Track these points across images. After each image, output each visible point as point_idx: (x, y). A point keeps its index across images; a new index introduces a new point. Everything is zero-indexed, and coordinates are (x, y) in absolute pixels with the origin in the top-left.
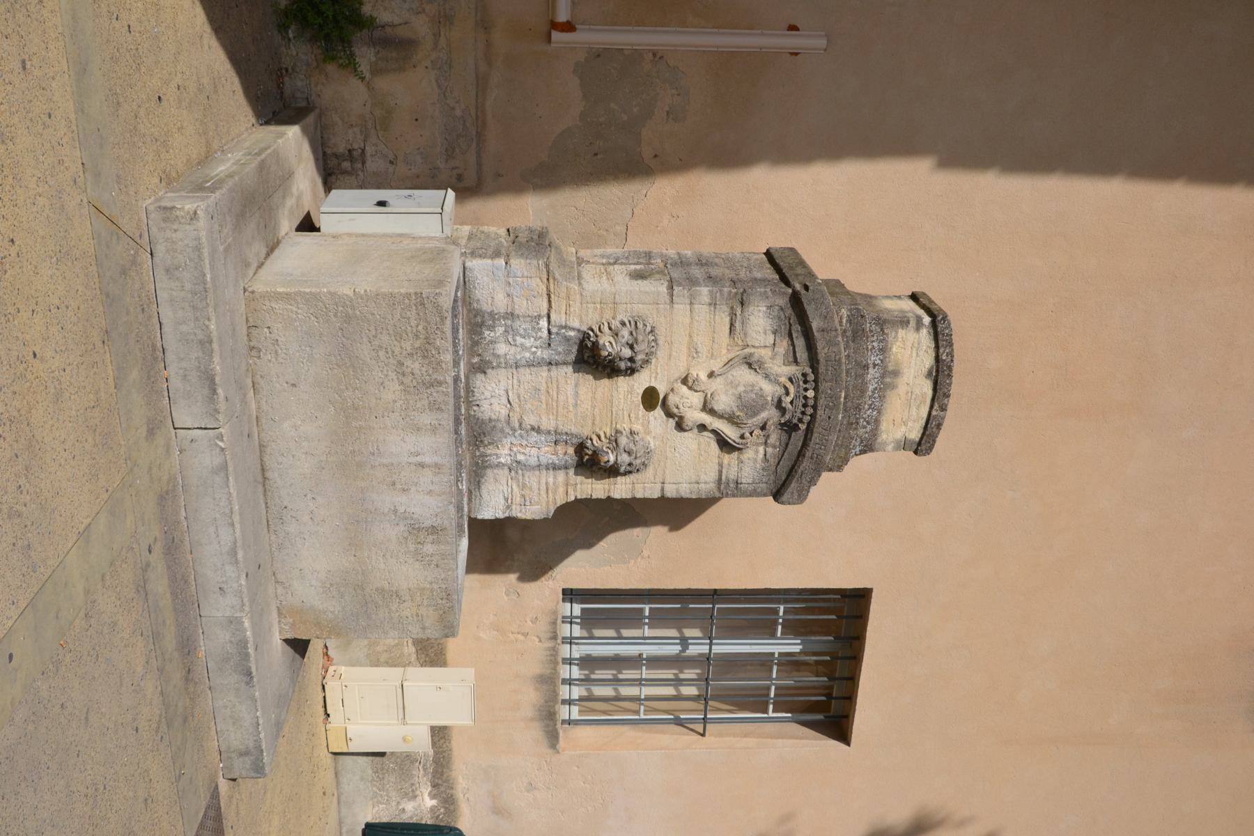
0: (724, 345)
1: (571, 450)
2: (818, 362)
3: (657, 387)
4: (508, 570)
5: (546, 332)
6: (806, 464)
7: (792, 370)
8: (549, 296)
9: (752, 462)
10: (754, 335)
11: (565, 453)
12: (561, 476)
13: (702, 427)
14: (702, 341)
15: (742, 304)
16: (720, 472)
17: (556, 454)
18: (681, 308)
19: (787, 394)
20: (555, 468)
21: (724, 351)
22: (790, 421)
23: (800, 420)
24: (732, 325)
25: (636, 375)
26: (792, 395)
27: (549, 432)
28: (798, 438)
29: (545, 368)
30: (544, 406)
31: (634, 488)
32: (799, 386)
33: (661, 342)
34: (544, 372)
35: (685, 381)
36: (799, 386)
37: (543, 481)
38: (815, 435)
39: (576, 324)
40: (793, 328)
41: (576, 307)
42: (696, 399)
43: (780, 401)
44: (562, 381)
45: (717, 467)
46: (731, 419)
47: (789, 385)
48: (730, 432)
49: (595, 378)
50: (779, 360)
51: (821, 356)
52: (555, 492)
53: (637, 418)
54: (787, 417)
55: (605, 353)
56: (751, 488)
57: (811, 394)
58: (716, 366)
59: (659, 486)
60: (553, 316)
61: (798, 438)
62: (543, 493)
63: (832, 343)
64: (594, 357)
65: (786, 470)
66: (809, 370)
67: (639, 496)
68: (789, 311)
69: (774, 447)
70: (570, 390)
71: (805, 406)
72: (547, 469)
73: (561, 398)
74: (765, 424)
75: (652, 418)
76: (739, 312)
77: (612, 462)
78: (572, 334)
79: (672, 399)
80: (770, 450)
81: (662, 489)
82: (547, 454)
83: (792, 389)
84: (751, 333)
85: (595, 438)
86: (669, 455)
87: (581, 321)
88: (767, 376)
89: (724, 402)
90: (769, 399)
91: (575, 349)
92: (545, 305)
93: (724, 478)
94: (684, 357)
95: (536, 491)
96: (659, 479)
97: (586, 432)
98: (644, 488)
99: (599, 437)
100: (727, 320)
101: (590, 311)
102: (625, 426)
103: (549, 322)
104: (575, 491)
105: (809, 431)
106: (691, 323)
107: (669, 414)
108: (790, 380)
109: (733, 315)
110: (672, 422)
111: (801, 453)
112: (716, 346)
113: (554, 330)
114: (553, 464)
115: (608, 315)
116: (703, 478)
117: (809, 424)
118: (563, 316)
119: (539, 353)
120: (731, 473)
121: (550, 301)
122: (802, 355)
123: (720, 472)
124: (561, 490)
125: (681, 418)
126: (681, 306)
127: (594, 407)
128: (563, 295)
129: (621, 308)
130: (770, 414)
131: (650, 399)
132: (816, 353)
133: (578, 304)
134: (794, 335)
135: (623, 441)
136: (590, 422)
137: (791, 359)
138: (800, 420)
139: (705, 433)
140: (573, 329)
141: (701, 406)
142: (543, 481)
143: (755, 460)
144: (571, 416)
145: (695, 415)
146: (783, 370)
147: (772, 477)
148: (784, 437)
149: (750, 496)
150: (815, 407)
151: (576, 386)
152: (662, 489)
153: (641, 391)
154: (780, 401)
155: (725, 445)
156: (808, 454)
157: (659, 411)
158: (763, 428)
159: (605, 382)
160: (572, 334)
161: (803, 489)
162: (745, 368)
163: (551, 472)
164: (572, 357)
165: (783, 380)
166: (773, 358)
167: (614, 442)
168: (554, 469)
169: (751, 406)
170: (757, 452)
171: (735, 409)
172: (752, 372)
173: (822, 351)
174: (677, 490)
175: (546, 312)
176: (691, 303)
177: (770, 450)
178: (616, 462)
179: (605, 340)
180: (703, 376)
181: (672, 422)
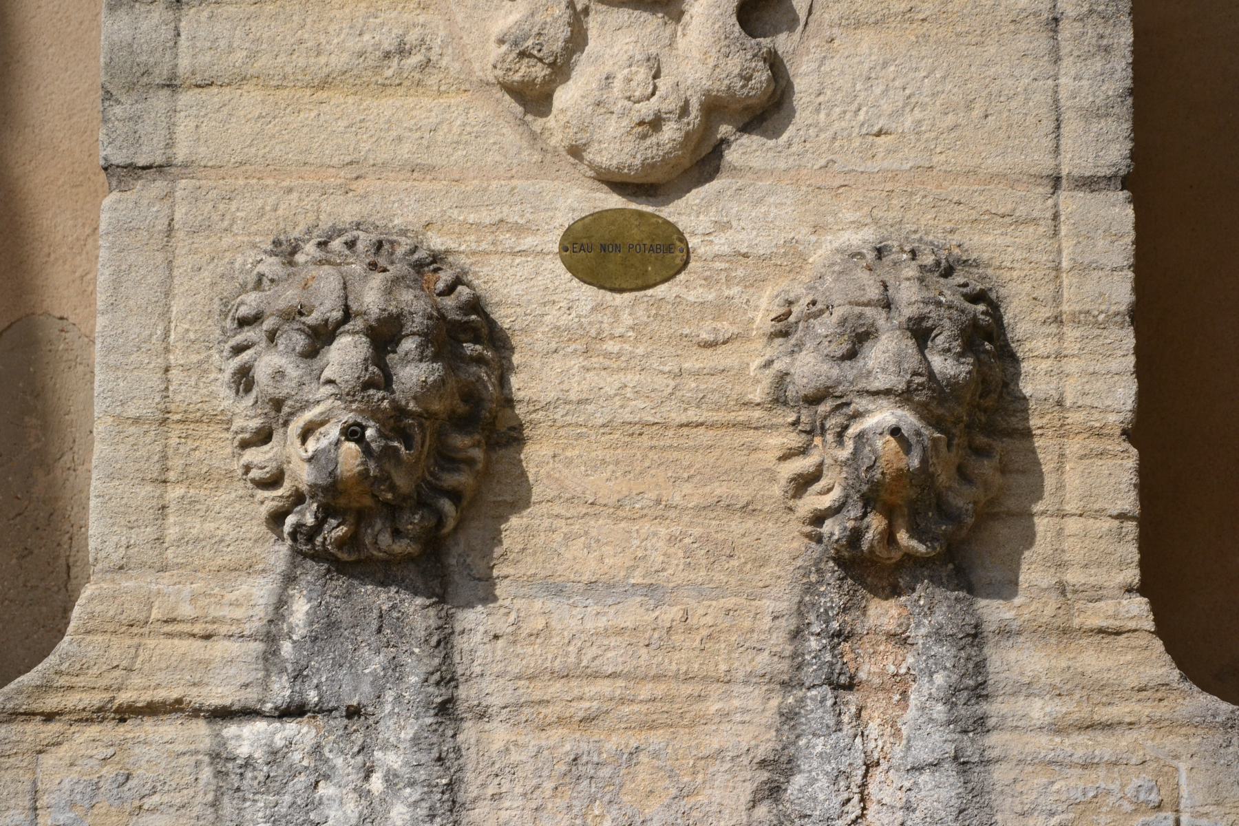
1: (884, 614)
3: (564, 220)
4: (781, 31)
5: (291, 727)
8: (125, 714)
11: (900, 639)
12: (1011, 662)
17: (900, 684)
18: (193, 127)
20: (972, 688)
25: (504, 317)
27: (789, 717)
29: (469, 732)
30: (657, 739)
31: (1082, 318)
33: (349, 212)
34: (487, 740)
35: (534, 99)
37: (1043, 744)
39: (258, 592)
41: (178, 595)
44: (532, 655)
49: (520, 502)
52: (1104, 690)
53: (721, 309)
55: (350, 456)
59: (1070, 201)
60: (219, 694)
62: (1105, 746)
64: (392, 511)
67: (1121, 292)
70: (570, 618)
72: (980, 724)
73: (614, 659)
75: (721, 244)
77: (908, 419)
78: (300, 609)
79: (616, 147)
81: (1089, 183)
82: (907, 722)
85: (815, 500)
86: (907, 159)
87: (248, 568)
91: (377, 598)
92: (167, 730)
94: (423, 109)
95: (1099, 778)
96: (1037, 202)
97: (786, 543)
98: (1083, 269)
99: (802, 483)
101: (197, 527)
102: (754, 366)
103: (248, 713)
104: (1096, 595)
106: (260, 80)
107: (702, 163)
110: (745, 151)
113: (281, 691)
114: (950, 697)
115: (218, 450)
118: (220, 648)
119: (392, 760)
121: (153, 710)
124: (1093, 660)
125: (714, 108)
126: (184, 128)
127: (663, 509)
128: (119, 648)
129: (184, 393)
131: (623, 252)
133: (164, 584)
135: (809, 367)
136: (737, 527)
140: (281, 604)
142: (1043, 744)
144: (706, 614)
151: (558, 591)
152: (1089, 183)
153: (587, 295)
157: (688, 213)
159: (536, 457)
160: (300, 609)
163: (995, 709)
164: (417, 612)
167: (821, 407)
168: (980, 692)
174: (1095, 113)
175: (201, 728)
176: (171, 85)
178: (904, 397)
179: (297, 459)
181: (745, 151)
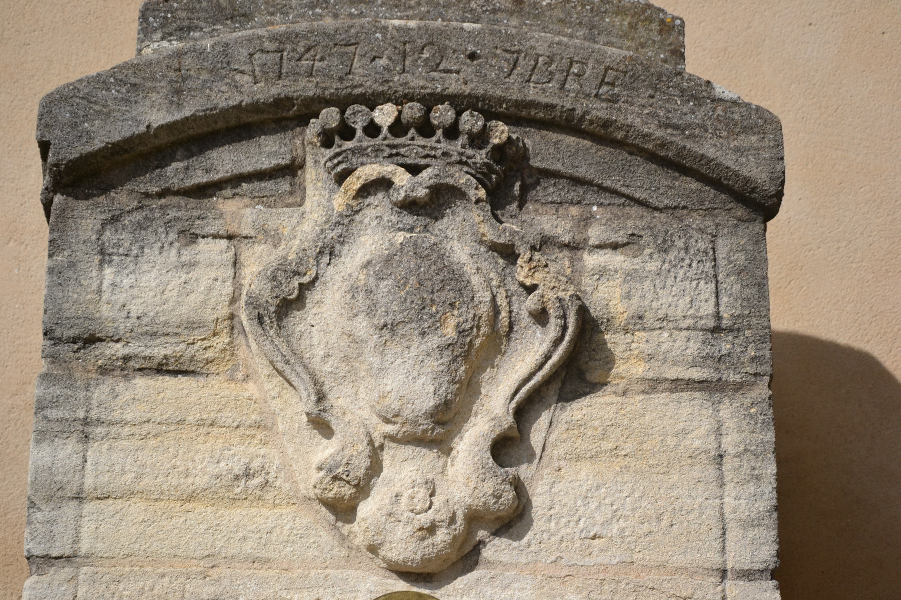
0: (231, 389)
2: (281, 103)
6: (636, 116)
7: (314, 177)
9: (647, 289)
10: (194, 299)
13: (506, 448)
14: (207, 460)
15: (91, 340)
16: (678, 385)
19: (384, 184)
21: (251, 388)
22: (482, 176)
23: (478, 139)
24: (161, 369)
26: (387, 169)
28: (544, 149)
32: (360, 151)
35: (343, 510)
36: (360, 151)
38: (532, 93)
40: (175, 182)
42: (404, 469)
43: (410, 206)
45: (661, 398)
46: (474, 353)
47: (354, 183)
48: (529, 354)
50: (281, 218)
51: (265, 91)
54: (462, 178)
56: (731, 285)
57: (385, 115)
58: (296, 406)
61: (544, 149)
63: (221, 65)
65: (663, 178)
66: (313, 128)
68: (122, 198)
69: (586, 220)
71: (425, 128)
74: (493, 247)
76: (119, 349)
80: (595, 234)
81: (747, 575)
83: (370, 171)
84: (188, 307)
86: (614, 556)
88: (329, 251)
89: (410, 379)
90: (400, 237)
93: (696, 374)
94: (263, 517)
100: (141, 383)
105: (520, 115)
108: (341, 178)
109: (126, 367)
110: (497, 549)
111: (602, 135)
112: (228, 416)
116: (699, 438)
117: (489, 115)
120: (681, 351)
122: (267, 151)
123: (678, 385)
125: (474, 518)
130: (460, 238)
132: (255, 107)
134: (200, 178)
137: (284, 185)
138: (478, 139)
139: (536, 437)
141: (428, 456)
143: (629, 276)
145: (464, 474)
146: (320, 199)
147: (695, 220)
148: (549, 191)
149: (762, 285)
150: (430, 101)
152: (747, 575)
154: (410, 206)
155: (578, 368)
156: (599, 110)
158: (508, 253)
161: (729, 124)
162: (297, 322)
165: (340, 201)
166: (274, 238)
169: (430, 289)
170: (602, 273)
171: (434, 341)
172: (312, 297)
173: (250, 89)
176: (79, 498)
177: (595, 234)
180: (325, 450)
181: (497, 549)
